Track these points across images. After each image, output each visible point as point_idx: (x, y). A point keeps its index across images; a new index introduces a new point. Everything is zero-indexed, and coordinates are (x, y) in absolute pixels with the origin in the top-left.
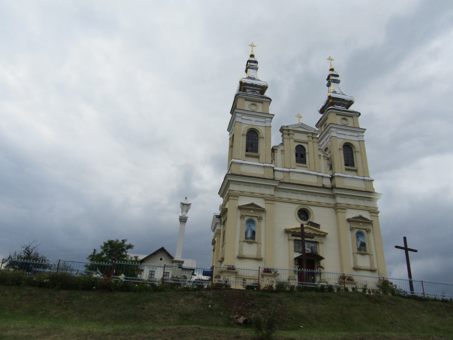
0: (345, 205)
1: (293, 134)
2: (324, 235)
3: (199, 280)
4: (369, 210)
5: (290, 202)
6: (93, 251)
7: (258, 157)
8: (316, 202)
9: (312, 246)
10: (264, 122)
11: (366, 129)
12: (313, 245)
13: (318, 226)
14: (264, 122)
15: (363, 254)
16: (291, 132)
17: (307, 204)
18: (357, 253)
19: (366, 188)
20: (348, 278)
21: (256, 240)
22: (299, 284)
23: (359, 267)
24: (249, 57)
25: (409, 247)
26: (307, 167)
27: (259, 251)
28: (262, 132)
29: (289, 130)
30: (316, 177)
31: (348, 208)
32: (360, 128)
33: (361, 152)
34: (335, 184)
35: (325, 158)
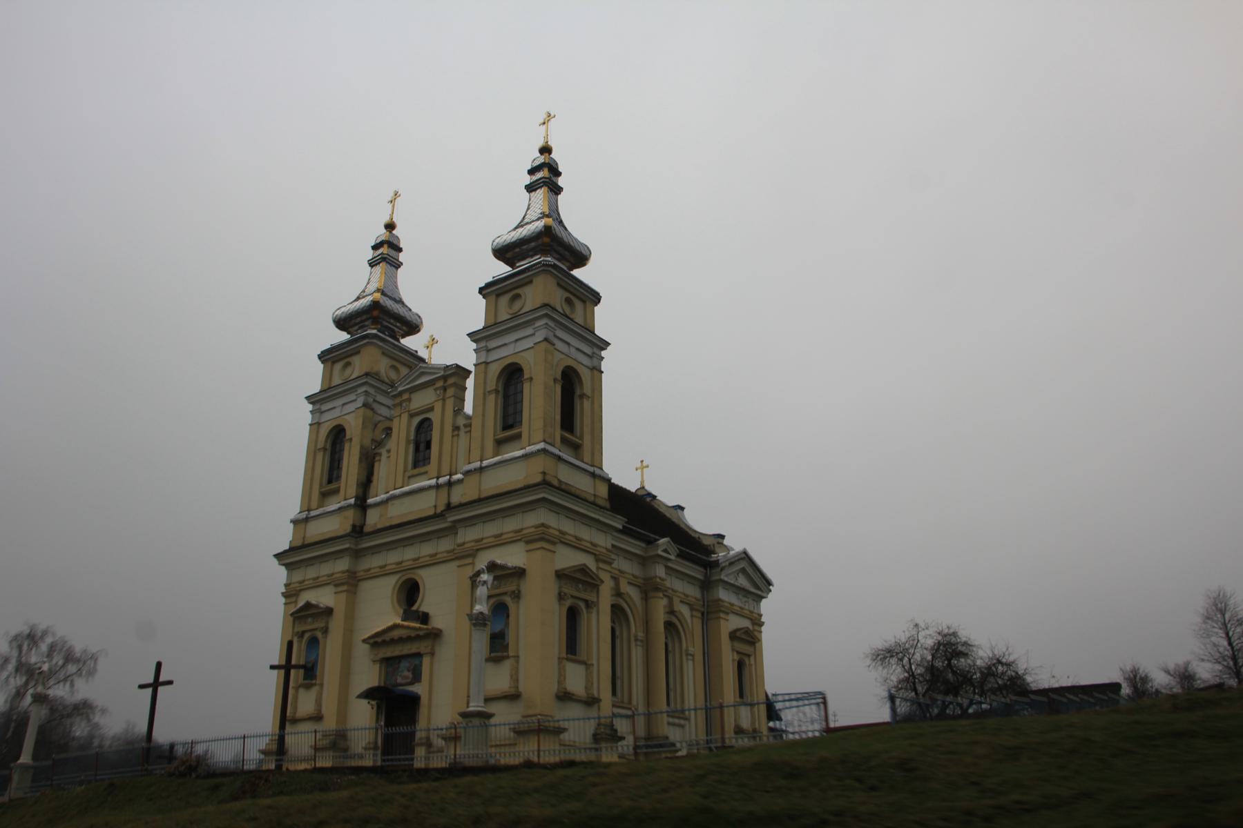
2: (436, 635)
3: (647, 748)
5: (402, 569)
6: (440, 727)
11: (610, 344)
20: (1013, 674)
22: (383, 761)
24: (529, 176)
25: (151, 680)
27: (515, 679)
28: (585, 374)
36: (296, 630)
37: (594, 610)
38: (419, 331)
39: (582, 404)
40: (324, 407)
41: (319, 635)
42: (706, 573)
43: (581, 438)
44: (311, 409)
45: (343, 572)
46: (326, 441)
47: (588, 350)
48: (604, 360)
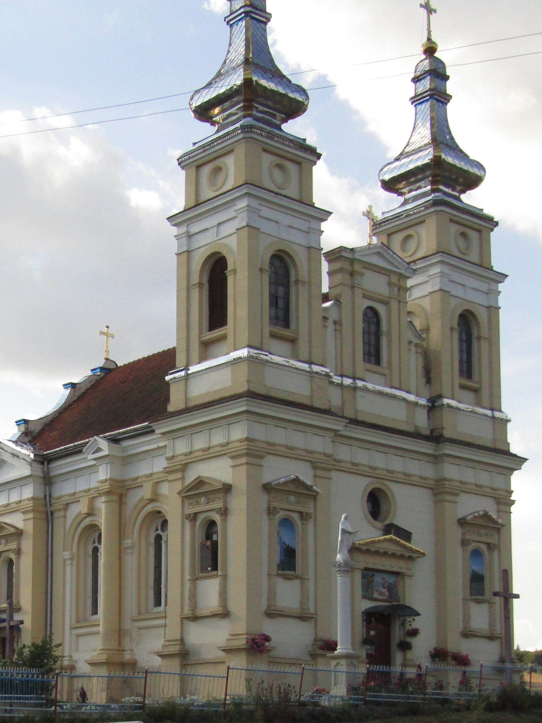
0: (264, 445)
1: (362, 274)
4: (314, 460)
7: (293, 341)
8: (367, 466)
9: (390, 583)
10: (305, 232)
12: (391, 579)
13: (407, 535)
14: (305, 232)
15: (288, 578)
16: (357, 267)
17: (403, 481)
18: (278, 575)
19: (495, 440)
21: (299, 570)
23: (279, 611)
26: (385, 375)
28: (482, 315)
29: (352, 261)
30: (403, 404)
31: (463, 491)
32: (316, 205)
33: (310, 285)
34: (443, 428)
35: (419, 350)
36: (187, 512)
37: (496, 553)
38: (305, 110)
39: (479, 347)
40: (195, 228)
41: (217, 518)
42: (43, 469)
43: (480, 382)
44: (176, 234)
45: (241, 441)
46: (201, 276)
47: (484, 287)
48: (501, 294)
